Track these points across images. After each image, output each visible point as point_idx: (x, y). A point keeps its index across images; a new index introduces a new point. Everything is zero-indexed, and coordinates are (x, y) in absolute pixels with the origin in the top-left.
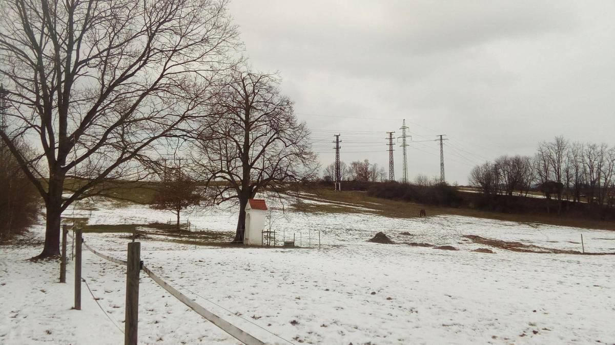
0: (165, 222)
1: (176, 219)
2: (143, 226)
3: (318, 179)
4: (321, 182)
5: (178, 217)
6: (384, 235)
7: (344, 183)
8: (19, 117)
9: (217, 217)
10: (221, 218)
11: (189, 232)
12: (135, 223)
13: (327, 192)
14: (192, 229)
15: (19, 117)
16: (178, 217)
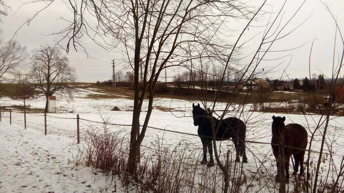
0: (19, 105)
1: (24, 104)
2: (9, 107)
3: (305, 79)
4: (107, 83)
5: (25, 103)
6: (117, 108)
7: (116, 83)
8: (275, 39)
9: (38, 103)
10: (39, 103)
11: (30, 109)
12: (5, 105)
13: (109, 88)
14: (31, 108)
15: (275, 39)
16: (25, 103)
